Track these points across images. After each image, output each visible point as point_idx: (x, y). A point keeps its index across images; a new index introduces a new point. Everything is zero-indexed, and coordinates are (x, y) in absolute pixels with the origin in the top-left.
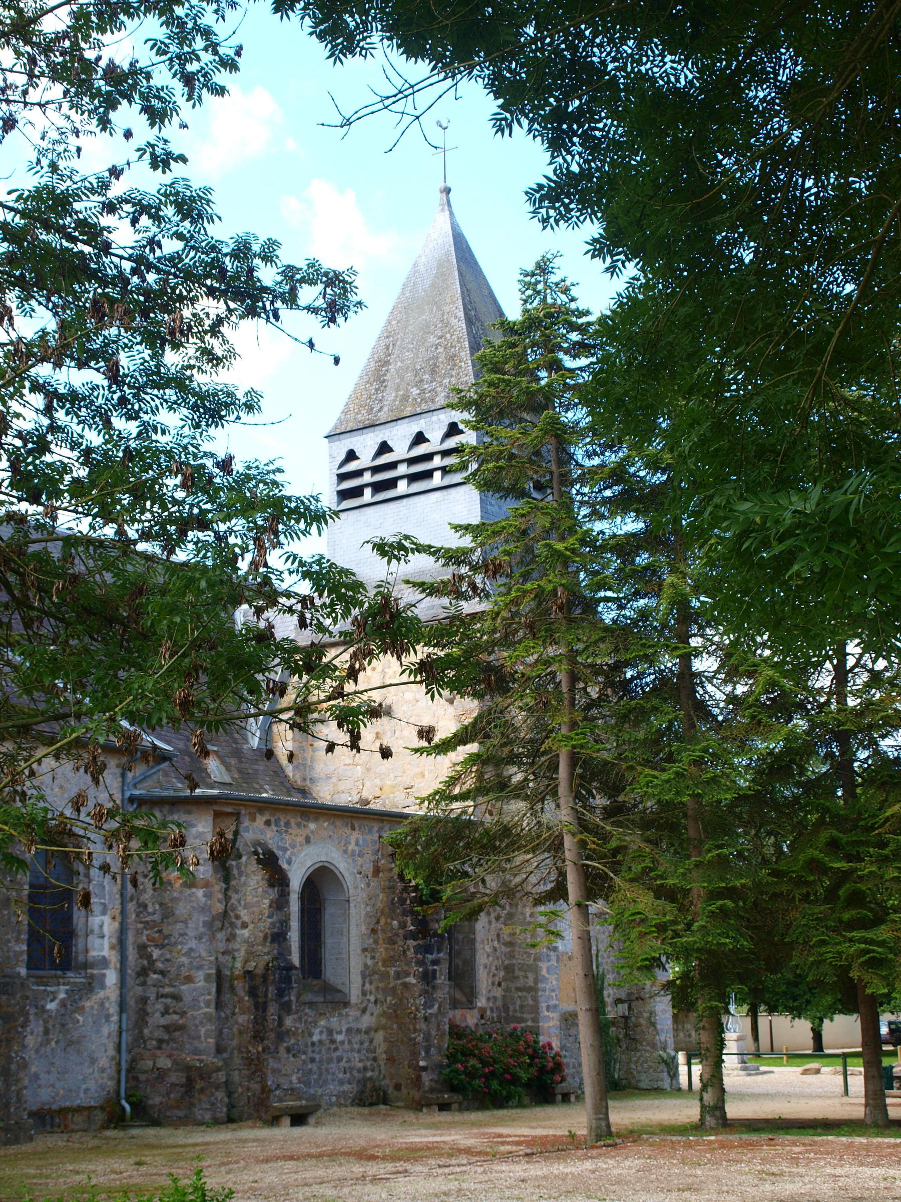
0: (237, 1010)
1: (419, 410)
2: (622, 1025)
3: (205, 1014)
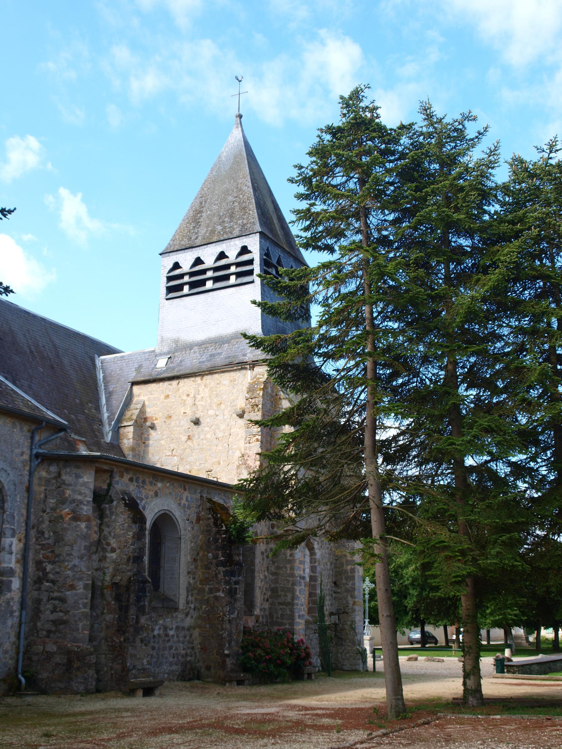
0: (105, 611)
1: (222, 238)
2: (333, 629)
3: (82, 613)
